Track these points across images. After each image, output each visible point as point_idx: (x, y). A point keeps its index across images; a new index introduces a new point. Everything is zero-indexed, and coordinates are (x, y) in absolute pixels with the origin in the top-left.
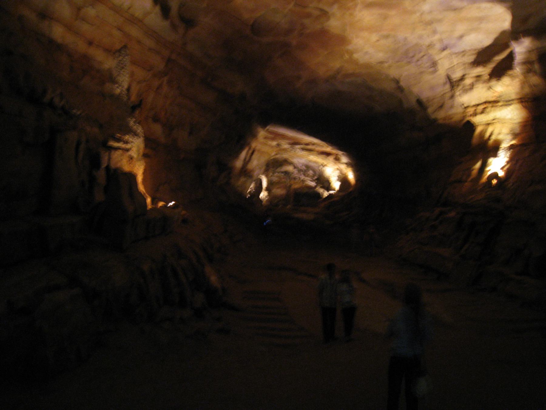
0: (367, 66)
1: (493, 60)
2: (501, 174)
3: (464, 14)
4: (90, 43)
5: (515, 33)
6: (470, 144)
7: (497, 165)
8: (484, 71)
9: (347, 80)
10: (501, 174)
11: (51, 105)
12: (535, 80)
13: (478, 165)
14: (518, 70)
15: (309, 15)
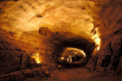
0: (77, 35)
1: (93, 31)
2: (98, 50)
3: (87, 25)
4: (30, 41)
5: (95, 27)
6: (93, 45)
7: (98, 48)
8: (93, 33)
9: (76, 38)
10: (98, 50)
11: (22, 51)
12: (100, 34)
13: (96, 49)
14: (97, 32)
15: (64, 30)
